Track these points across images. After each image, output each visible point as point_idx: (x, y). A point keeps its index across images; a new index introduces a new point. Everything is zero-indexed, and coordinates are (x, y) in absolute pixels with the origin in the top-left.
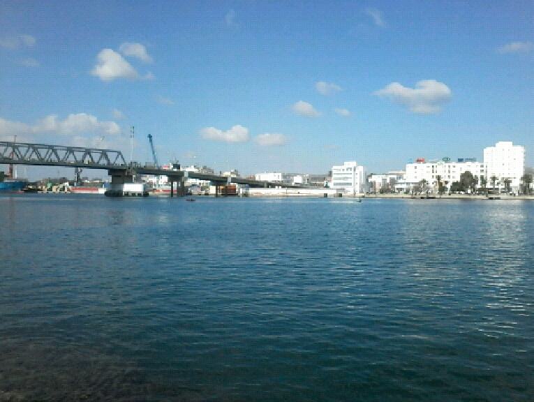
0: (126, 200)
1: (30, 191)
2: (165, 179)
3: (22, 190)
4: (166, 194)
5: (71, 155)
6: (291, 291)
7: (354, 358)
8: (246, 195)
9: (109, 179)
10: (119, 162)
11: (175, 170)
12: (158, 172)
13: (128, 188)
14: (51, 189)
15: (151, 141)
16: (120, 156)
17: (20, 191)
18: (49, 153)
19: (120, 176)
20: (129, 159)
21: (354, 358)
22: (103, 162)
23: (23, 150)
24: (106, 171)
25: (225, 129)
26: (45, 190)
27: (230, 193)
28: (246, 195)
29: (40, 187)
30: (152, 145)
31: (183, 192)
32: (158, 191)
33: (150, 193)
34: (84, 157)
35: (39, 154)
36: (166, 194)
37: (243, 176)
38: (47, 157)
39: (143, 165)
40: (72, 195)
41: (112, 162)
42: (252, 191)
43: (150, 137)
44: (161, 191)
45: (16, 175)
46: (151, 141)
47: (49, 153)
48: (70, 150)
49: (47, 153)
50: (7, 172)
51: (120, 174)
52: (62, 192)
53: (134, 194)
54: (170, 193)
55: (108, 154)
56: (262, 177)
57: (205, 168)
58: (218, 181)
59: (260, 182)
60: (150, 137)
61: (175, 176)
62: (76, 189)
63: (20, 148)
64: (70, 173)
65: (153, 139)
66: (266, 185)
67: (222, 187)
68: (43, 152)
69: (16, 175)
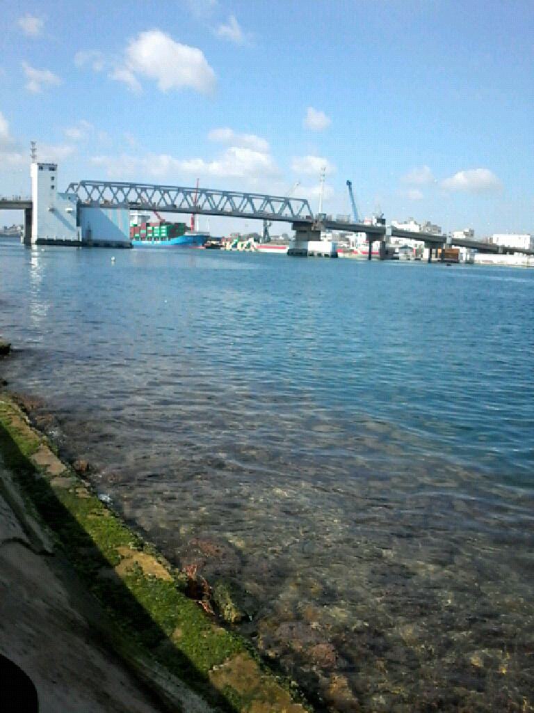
0: (309, 259)
1: (213, 247)
2: (362, 237)
3: (203, 245)
4: (364, 257)
5: (269, 205)
6: (337, 401)
7: (487, 529)
8: (470, 262)
9: (292, 234)
10: (304, 214)
11: (379, 225)
12: (356, 229)
13: (312, 246)
14: (235, 246)
15: (350, 189)
16: (306, 206)
17: (201, 247)
18: (244, 204)
19: (305, 231)
20: (317, 210)
21: (487, 529)
22: (287, 212)
23: (217, 198)
24: (290, 225)
25: (208, 161)
26: (229, 247)
27: (450, 258)
28: (470, 262)
29: (223, 244)
30: (351, 194)
31: (387, 254)
32: (356, 253)
33: (340, 255)
34: (282, 209)
35: (232, 204)
36: (364, 257)
37: (478, 238)
38: (242, 207)
39: (334, 219)
40: (258, 254)
41: (296, 212)
42: (480, 258)
43: (349, 183)
44: (359, 252)
45: (198, 228)
46: (350, 189)
47: (244, 204)
48: (248, 197)
49: (242, 203)
50: (189, 225)
51: (306, 228)
52: (248, 250)
53: (320, 255)
54: (368, 255)
55: (292, 202)
56: (501, 240)
57: (428, 224)
58: (433, 242)
59: (495, 246)
60: (349, 183)
61: (374, 234)
62: (261, 247)
63: (214, 196)
64: (257, 226)
65: (352, 186)
66: (500, 251)
67: (440, 251)
68: (237, 201)
69: (198, 228)
